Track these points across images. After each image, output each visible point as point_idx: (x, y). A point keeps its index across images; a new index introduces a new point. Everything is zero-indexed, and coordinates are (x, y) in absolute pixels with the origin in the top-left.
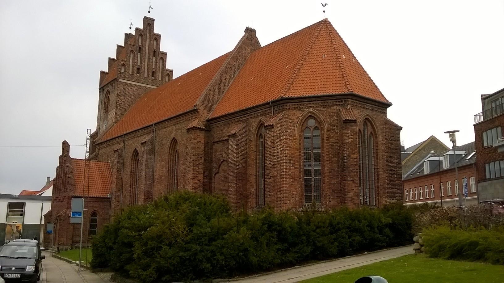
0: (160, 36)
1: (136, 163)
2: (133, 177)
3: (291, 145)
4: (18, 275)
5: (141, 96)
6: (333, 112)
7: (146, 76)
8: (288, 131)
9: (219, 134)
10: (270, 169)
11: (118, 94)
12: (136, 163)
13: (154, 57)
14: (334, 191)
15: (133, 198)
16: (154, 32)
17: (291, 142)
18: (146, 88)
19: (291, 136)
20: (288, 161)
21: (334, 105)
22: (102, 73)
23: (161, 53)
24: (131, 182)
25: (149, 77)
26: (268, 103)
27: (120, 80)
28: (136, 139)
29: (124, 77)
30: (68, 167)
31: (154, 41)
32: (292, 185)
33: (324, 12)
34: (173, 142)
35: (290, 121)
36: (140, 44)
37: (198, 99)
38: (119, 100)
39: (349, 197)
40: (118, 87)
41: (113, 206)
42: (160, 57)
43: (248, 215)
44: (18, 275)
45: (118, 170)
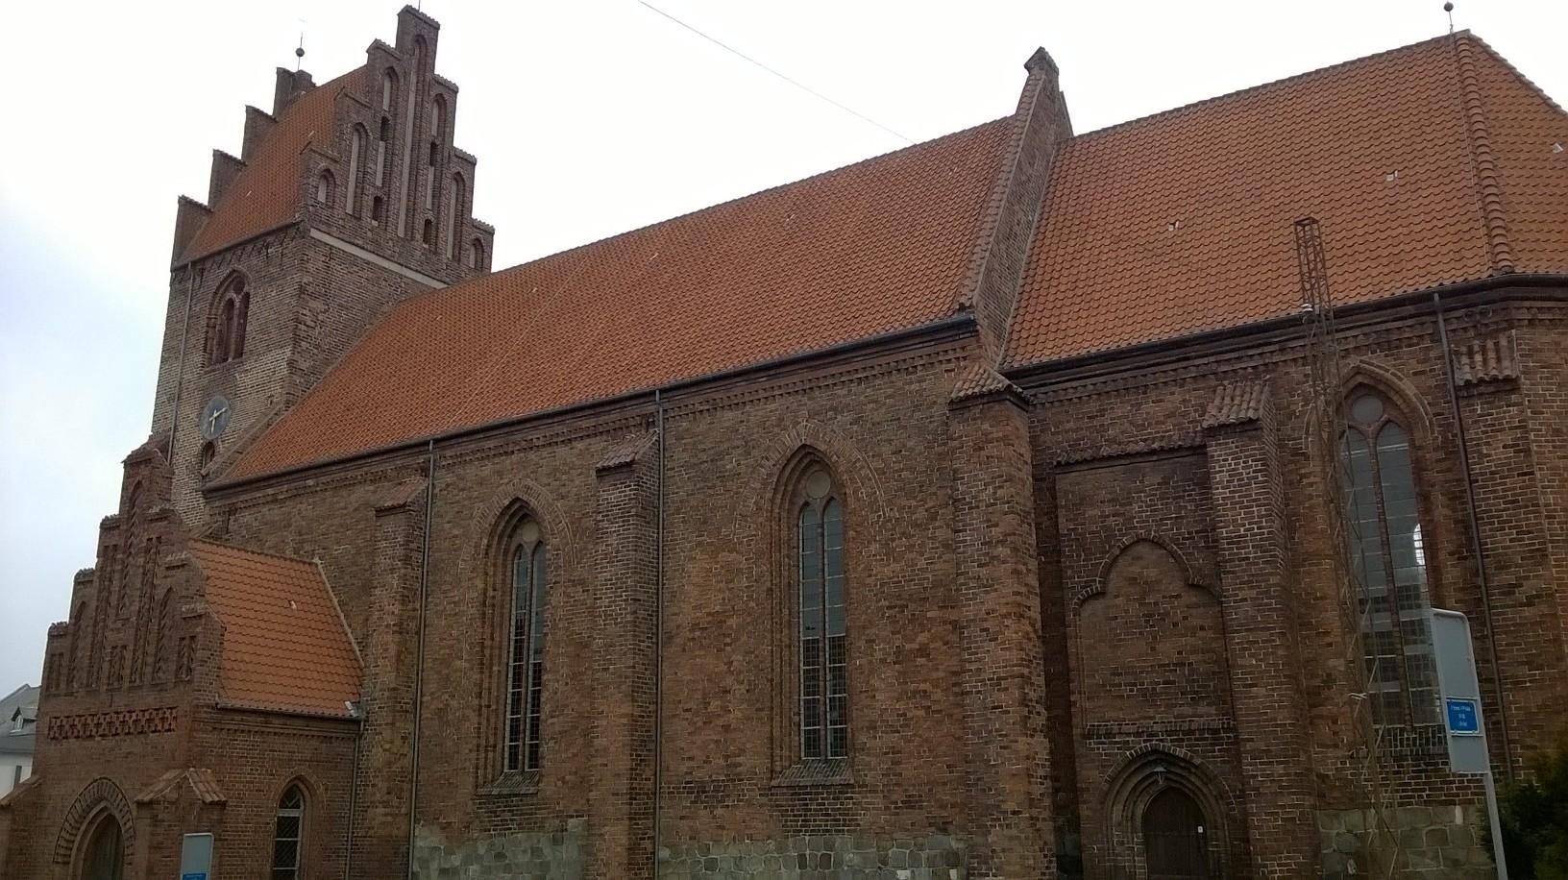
0: (457, 92)
1: (505, 566)
2: (492, 626)
5: (385, 308)
7: (401, 234)
8: (1543, 413)
9: (1076, 431)
11: (302, 290)
12: (505, 566)
13: (431, 165)
15: (493, 720)
16: (436, 72)
18: (405, 280)
20: (1561, 535)
22: (186, 205)
23: (457, 156)
24: (483, 647)
26: (1425, 297)
27: (314, 233)
29: (329, 225)
30: (183, 566)
31: (433, 104)
34: (792, 465)
35: (1543, 372)
38: (304, 312)
40: (305, 258)
41: (377, 757)
42: (454, 170)
43: (1323, 778)
45: (406, 592)
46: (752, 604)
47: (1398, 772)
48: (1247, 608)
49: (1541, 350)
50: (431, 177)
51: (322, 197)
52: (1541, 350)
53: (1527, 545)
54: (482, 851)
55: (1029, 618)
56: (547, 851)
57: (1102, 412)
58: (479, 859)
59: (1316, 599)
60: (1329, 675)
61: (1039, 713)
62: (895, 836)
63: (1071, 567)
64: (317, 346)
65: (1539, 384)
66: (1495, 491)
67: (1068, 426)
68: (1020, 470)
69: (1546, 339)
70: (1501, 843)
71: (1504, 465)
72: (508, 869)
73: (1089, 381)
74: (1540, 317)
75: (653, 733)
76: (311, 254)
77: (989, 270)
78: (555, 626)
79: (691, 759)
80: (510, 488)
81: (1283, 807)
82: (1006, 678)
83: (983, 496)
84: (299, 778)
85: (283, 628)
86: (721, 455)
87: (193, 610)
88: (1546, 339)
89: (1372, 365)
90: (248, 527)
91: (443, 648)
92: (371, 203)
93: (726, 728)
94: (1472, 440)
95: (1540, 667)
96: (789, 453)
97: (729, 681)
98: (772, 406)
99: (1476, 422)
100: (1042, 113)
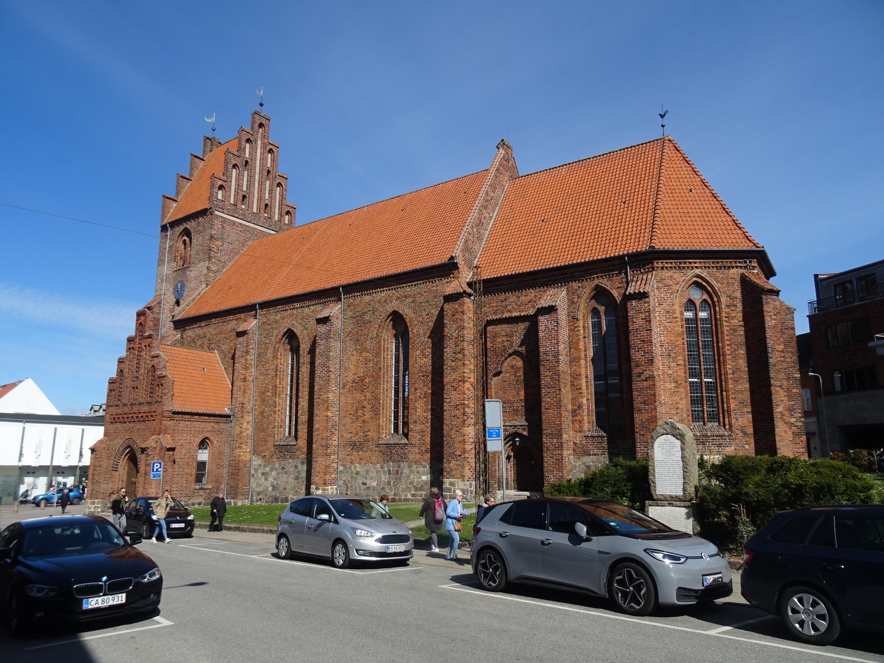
3: (670, 327)
4: (120, 599)
6: (732, 278)
7: (255, 211)
9: (496, 307)
10: (643, 366)
11: (212, 237)
14: (742, 403)
17: (670, 322)
19: (668, 312)
21: (733, 267)
25: (260, 212)
27: (217, 213)
28: (289, 312)
32: (674, 392)
33: (663, 126)
36: (247, 155)
37: (457, 247)
39: (779, 412)
44: (120, 599)
46: (374, 373)
47: (601, 442)
48: (548, 379)
49: (665, 279)
50: (268, 185)
51: (220, 197)
52: (665, 279)
53: (647, 358)
54: (277, 466)
55: (470, 382)
56: (299, 467)
57: (506, 300)
58: (276, 469)
59: (577, 375)
60: (580, 405)
61: (472, 418)
62: (422, 463)
63: (491, 361)
64: (219, 260)
65: (662, 293)
66: (637, 336)
67: (493, 305)
68: (469, 324)
69: (668, 275)
70: (180, 526)
71: (641, 326)
72: (286, 473)
73: (501, 287)
74: (666, 265)
75: (337, 422)
76: (216, 221)
77: (466, 241)
78: (303, 380)
79: (351, 433)
80: (286, 325)
81: (556, 455)
82: (459, 405)
83: (454, 334)
84: (206, 438)
85: (200, 379)
86: (364, 313)
87: (162, 374)
88: (668, 275)
89: (602, 283)
90: (190, 337)
91: (262, 388)
92: (241, 198)
93: (364, 421)
94: (630, 316)
95: (648, 405)
96: (388, 314)
97: (365, 403)
98: (383, 295)
99: (633, 309)
100: (501, 168)
